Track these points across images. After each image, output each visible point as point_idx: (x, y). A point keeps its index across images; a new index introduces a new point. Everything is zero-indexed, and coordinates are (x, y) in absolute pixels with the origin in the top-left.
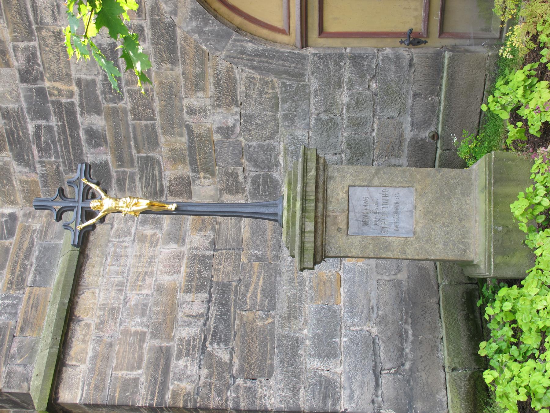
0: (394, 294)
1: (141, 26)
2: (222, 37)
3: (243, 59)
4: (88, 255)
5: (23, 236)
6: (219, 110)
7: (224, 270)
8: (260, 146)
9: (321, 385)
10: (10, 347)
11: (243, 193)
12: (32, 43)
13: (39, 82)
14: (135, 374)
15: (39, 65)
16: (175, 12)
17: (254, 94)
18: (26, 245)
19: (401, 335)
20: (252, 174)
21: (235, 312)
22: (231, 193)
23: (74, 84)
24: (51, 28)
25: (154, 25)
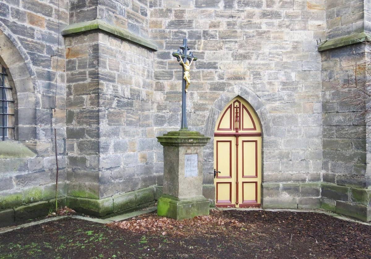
0: (131, 173)
1: (224, 79)
2: (220, 107)
3: (212, 114)
4: (139, 47)
5: (141, 19)
6: (192, 104)
7: (136, 104)
8: (178, 119)
9: (107, 146)
10: (111, 11)
11: (158, 112)
12: (218, 38)
13: (203, 38)
14: (108, 67)
15: (210, 39)
16: (228, 91)
17: (199, 118)
18: (139, 20)
19: (121, 177)
20: (166, 115)
21: (126, 109)
22: (157, 107)
23: (203, 51)
24: (223, 46)
25: (224, 83)
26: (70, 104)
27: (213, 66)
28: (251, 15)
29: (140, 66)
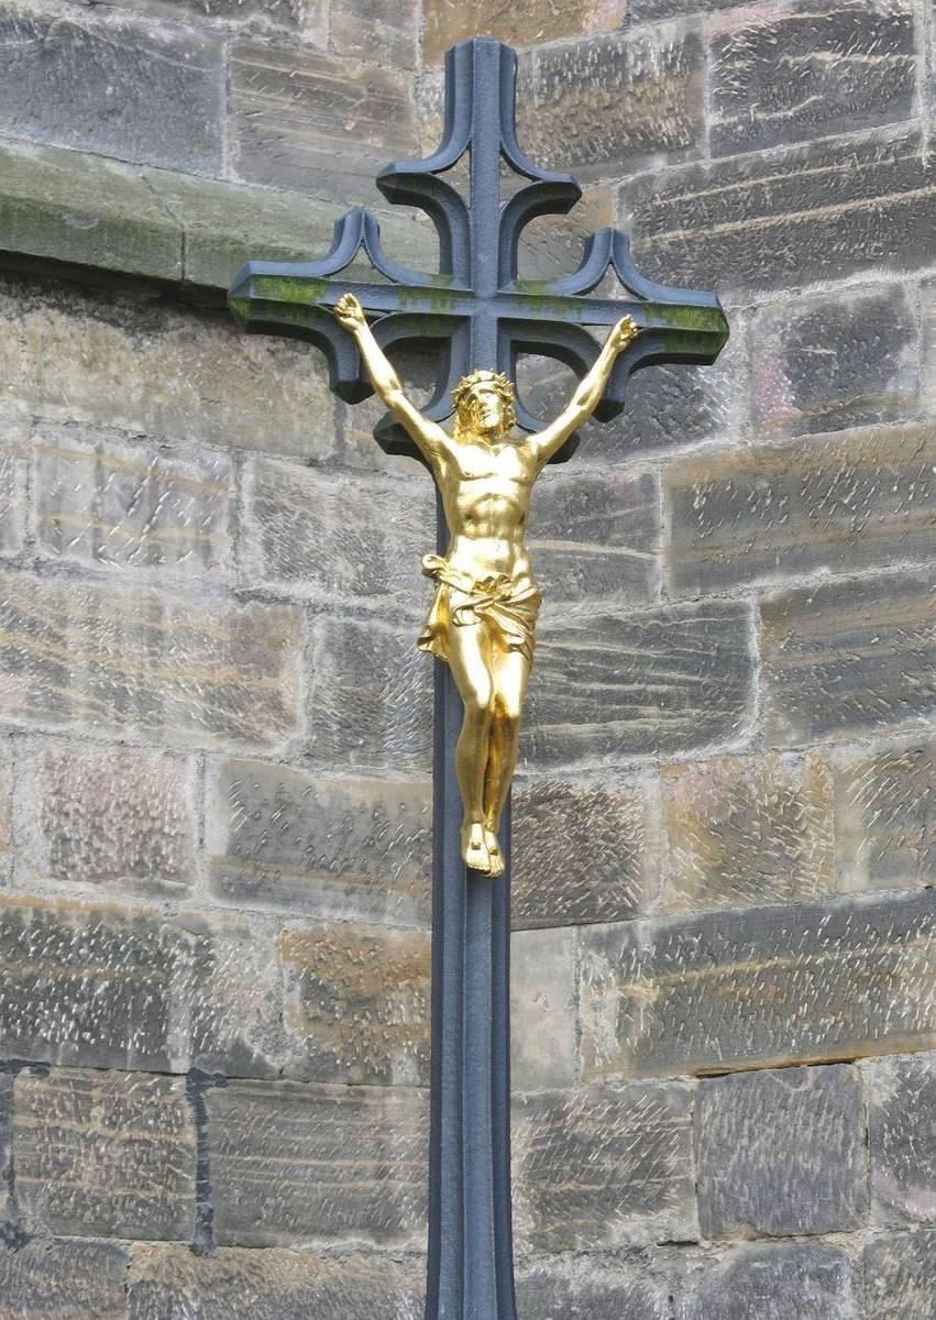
4: (154, 328)
20: (657, 1294)
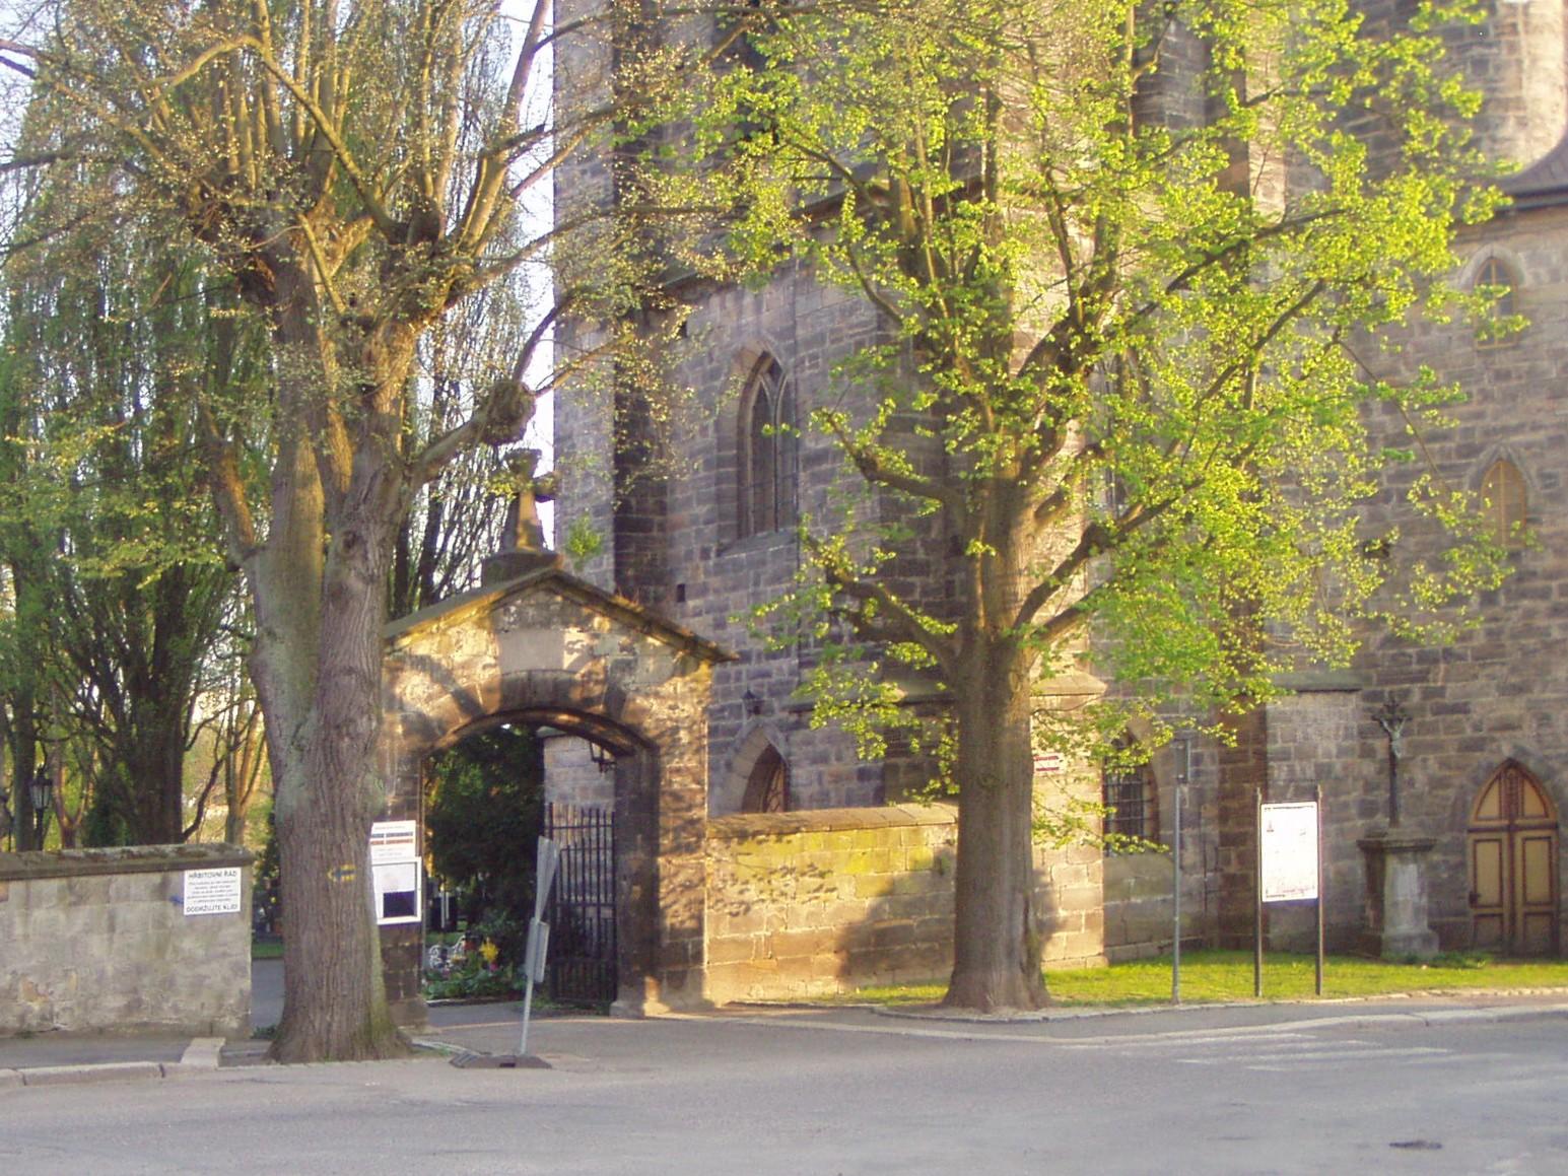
25: (1483, 739)
26: (1223, 796)
27: (1462, 709)
28: (1530, 614)
29: (1330, 724)
